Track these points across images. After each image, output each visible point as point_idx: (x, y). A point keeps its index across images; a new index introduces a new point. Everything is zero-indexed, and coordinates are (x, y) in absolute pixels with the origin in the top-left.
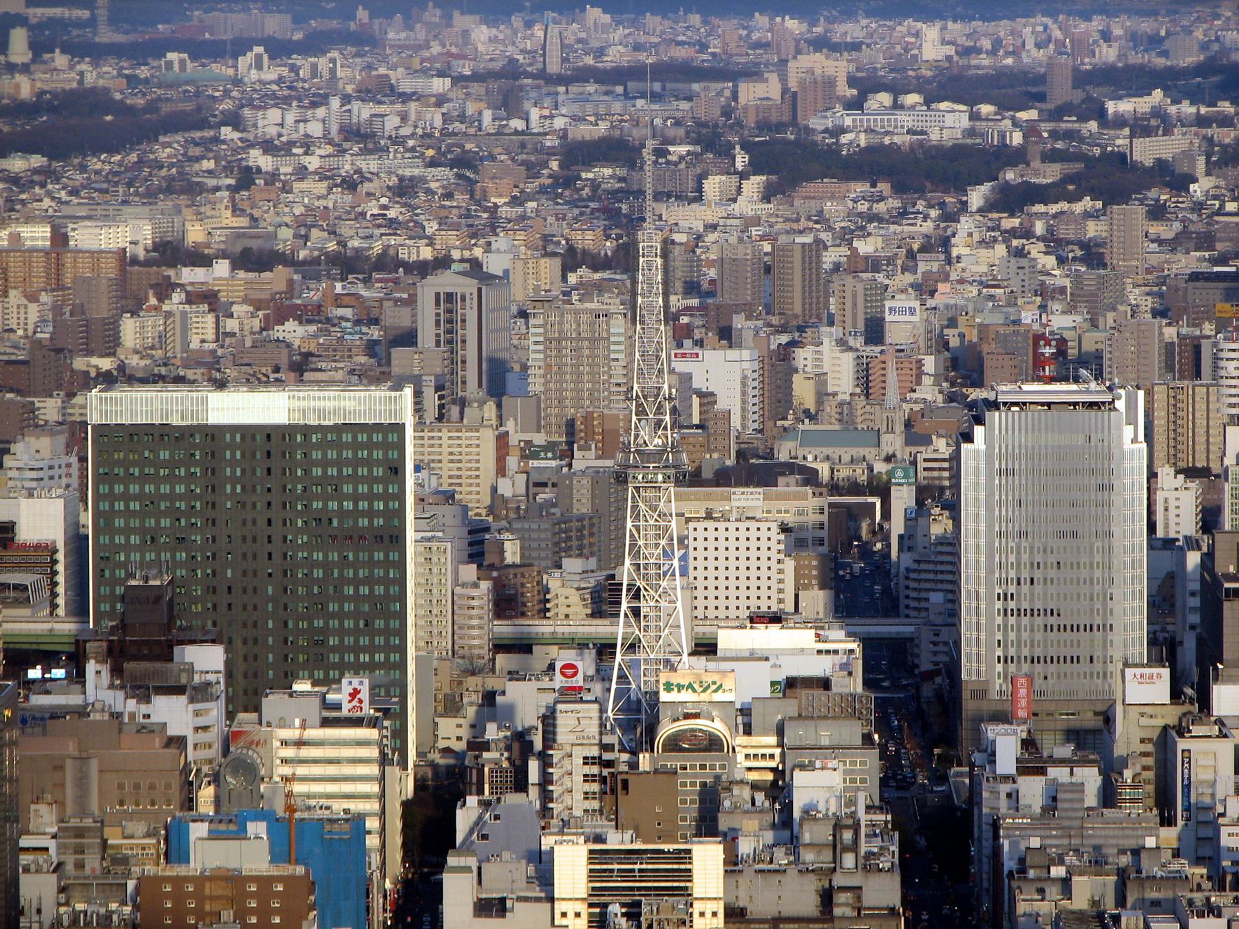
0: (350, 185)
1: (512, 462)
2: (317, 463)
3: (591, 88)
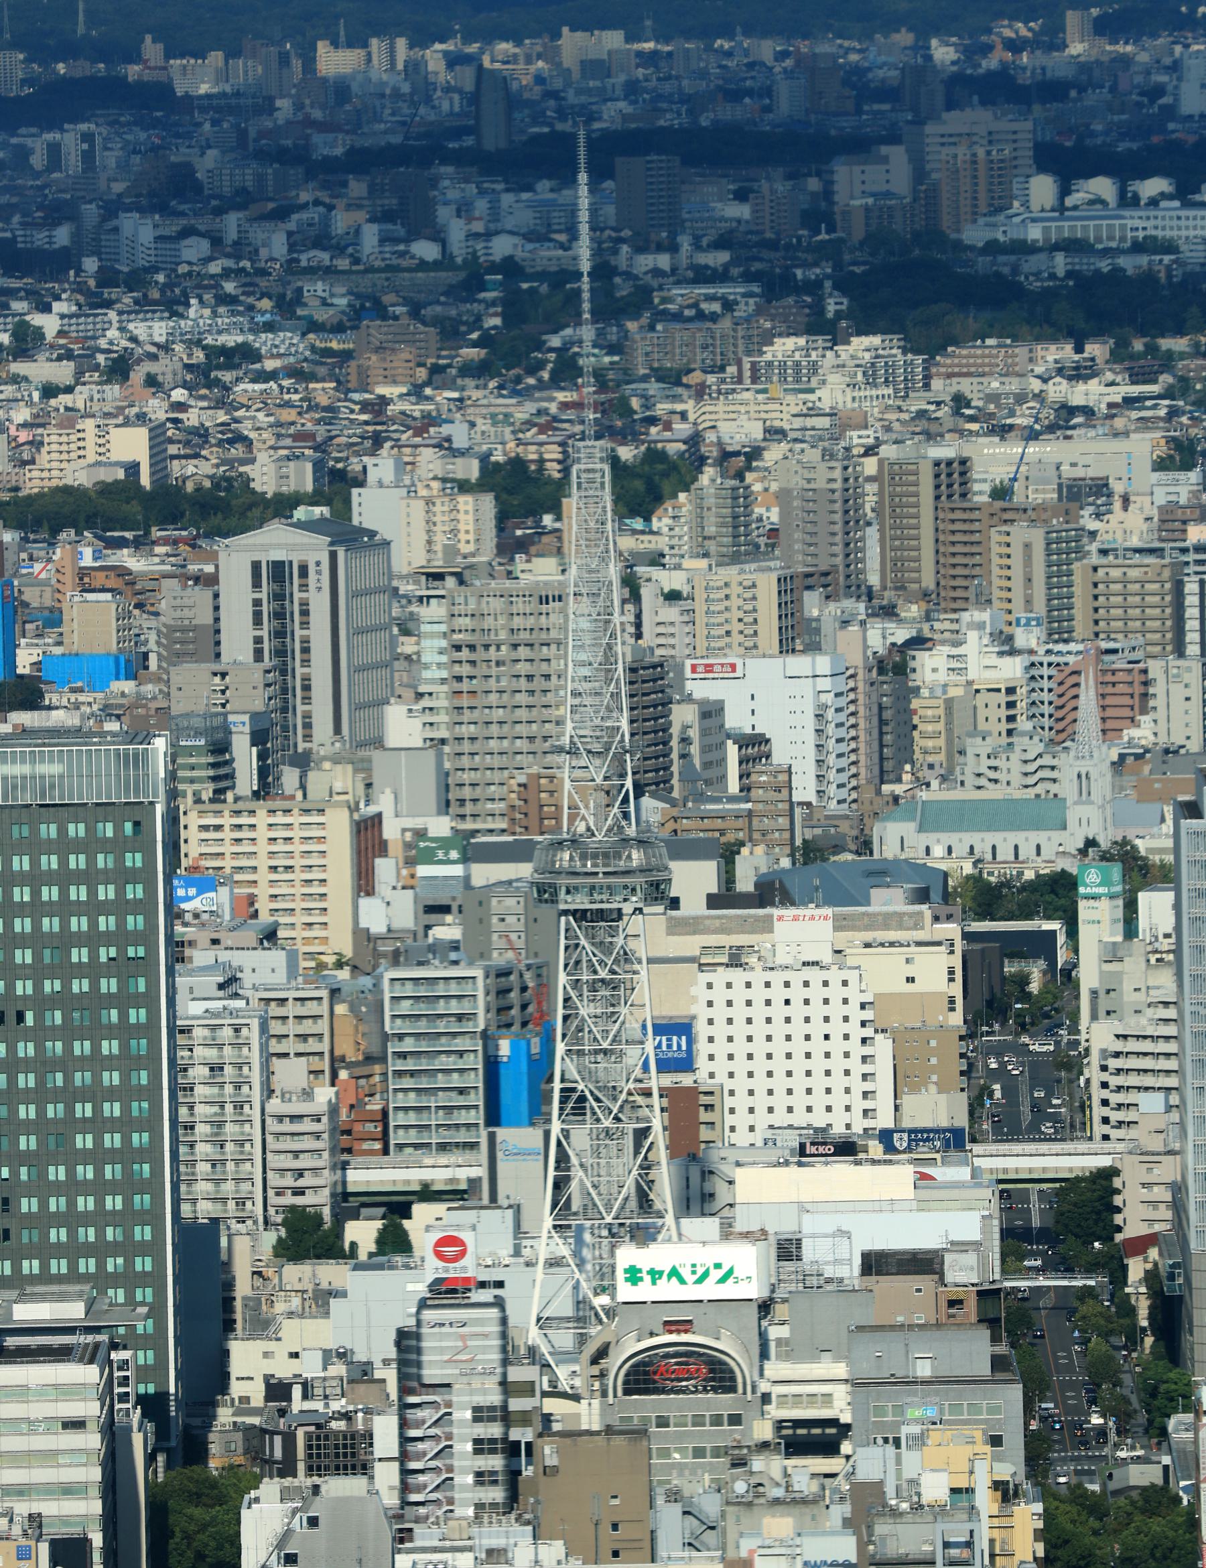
1: (385, 869)
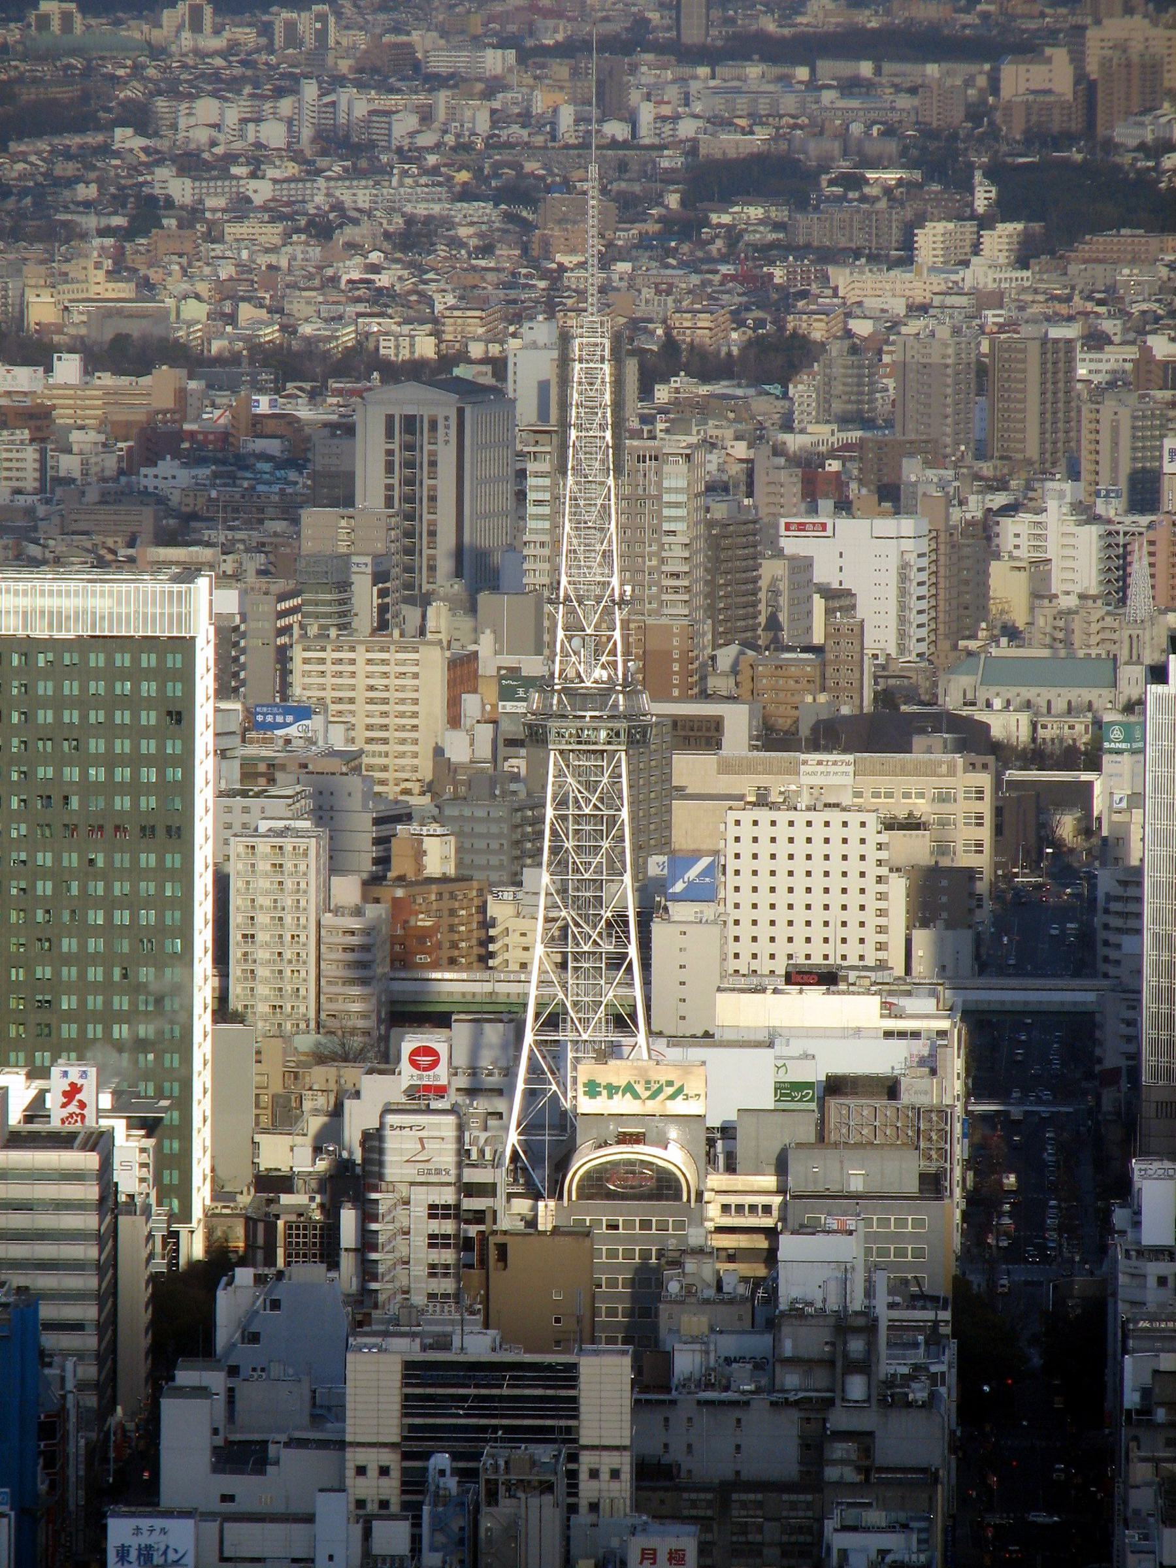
0: (321, 229)
2: (45, 703)
3: (754, 71)
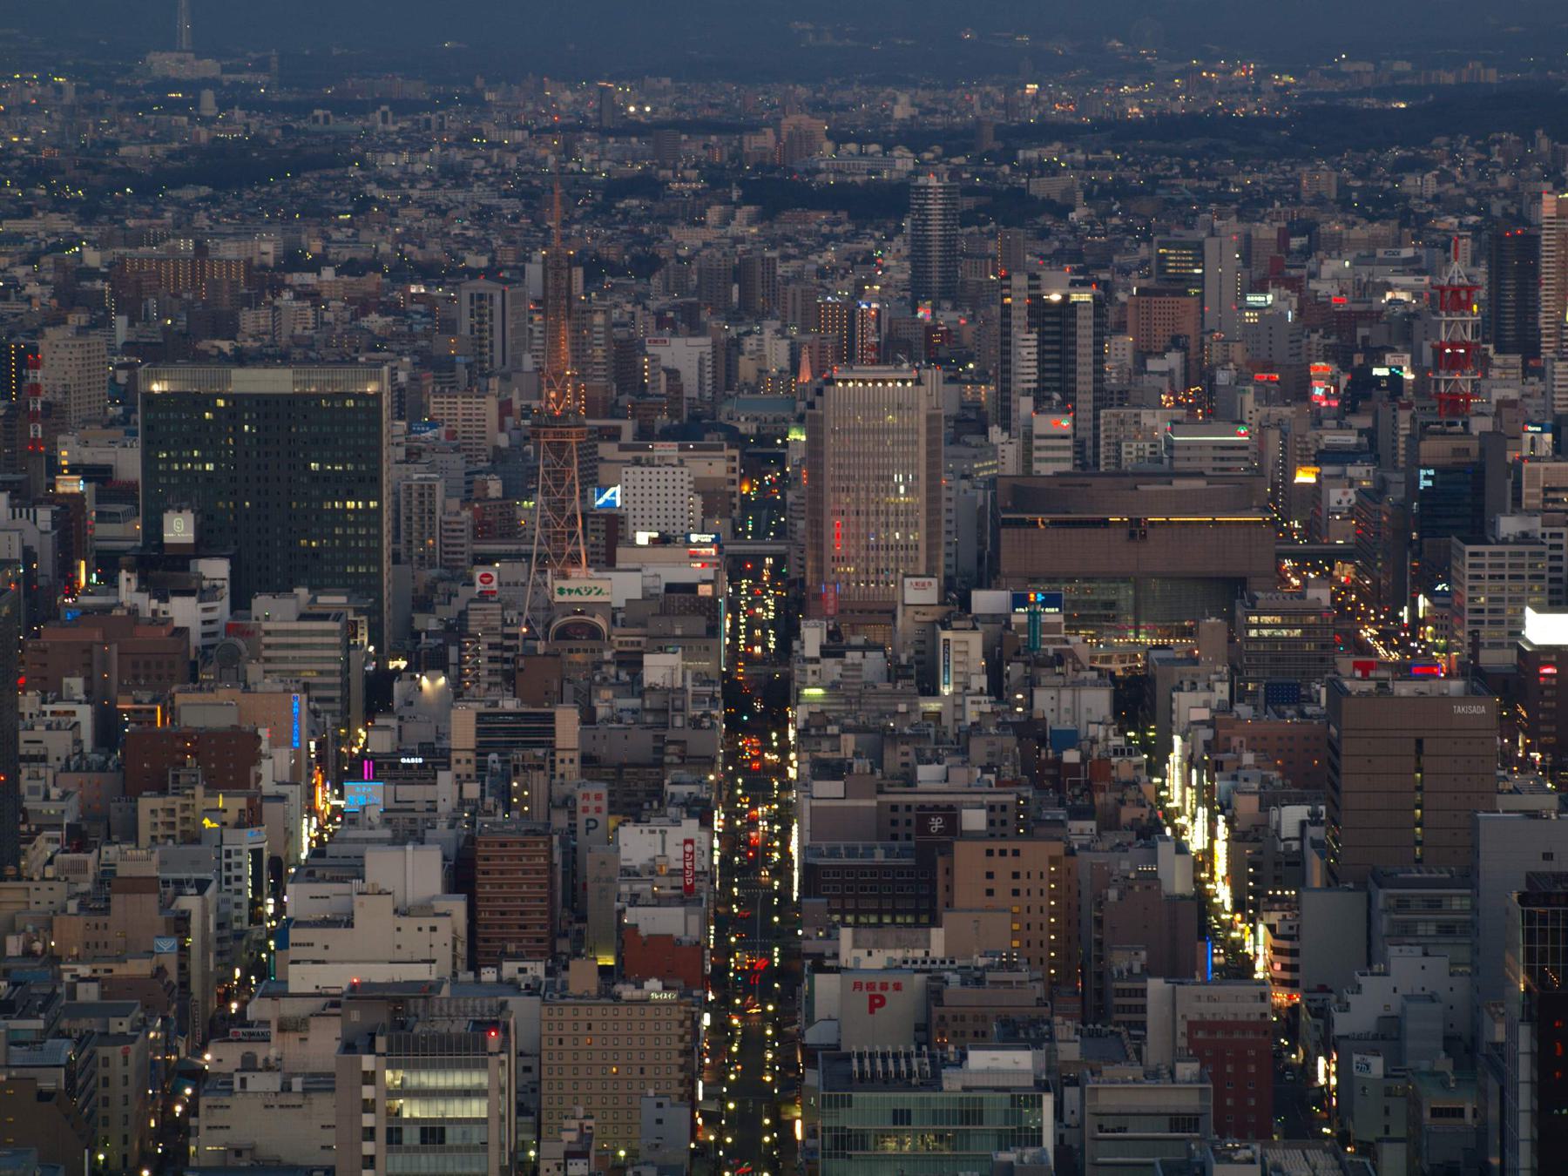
0: (441, 212)
